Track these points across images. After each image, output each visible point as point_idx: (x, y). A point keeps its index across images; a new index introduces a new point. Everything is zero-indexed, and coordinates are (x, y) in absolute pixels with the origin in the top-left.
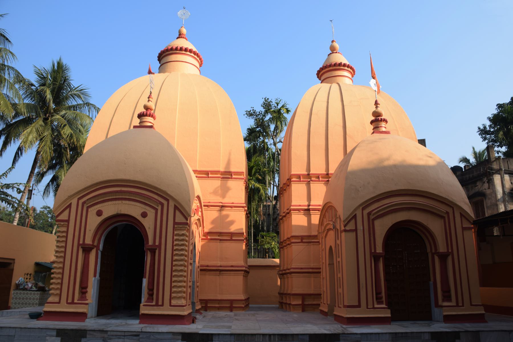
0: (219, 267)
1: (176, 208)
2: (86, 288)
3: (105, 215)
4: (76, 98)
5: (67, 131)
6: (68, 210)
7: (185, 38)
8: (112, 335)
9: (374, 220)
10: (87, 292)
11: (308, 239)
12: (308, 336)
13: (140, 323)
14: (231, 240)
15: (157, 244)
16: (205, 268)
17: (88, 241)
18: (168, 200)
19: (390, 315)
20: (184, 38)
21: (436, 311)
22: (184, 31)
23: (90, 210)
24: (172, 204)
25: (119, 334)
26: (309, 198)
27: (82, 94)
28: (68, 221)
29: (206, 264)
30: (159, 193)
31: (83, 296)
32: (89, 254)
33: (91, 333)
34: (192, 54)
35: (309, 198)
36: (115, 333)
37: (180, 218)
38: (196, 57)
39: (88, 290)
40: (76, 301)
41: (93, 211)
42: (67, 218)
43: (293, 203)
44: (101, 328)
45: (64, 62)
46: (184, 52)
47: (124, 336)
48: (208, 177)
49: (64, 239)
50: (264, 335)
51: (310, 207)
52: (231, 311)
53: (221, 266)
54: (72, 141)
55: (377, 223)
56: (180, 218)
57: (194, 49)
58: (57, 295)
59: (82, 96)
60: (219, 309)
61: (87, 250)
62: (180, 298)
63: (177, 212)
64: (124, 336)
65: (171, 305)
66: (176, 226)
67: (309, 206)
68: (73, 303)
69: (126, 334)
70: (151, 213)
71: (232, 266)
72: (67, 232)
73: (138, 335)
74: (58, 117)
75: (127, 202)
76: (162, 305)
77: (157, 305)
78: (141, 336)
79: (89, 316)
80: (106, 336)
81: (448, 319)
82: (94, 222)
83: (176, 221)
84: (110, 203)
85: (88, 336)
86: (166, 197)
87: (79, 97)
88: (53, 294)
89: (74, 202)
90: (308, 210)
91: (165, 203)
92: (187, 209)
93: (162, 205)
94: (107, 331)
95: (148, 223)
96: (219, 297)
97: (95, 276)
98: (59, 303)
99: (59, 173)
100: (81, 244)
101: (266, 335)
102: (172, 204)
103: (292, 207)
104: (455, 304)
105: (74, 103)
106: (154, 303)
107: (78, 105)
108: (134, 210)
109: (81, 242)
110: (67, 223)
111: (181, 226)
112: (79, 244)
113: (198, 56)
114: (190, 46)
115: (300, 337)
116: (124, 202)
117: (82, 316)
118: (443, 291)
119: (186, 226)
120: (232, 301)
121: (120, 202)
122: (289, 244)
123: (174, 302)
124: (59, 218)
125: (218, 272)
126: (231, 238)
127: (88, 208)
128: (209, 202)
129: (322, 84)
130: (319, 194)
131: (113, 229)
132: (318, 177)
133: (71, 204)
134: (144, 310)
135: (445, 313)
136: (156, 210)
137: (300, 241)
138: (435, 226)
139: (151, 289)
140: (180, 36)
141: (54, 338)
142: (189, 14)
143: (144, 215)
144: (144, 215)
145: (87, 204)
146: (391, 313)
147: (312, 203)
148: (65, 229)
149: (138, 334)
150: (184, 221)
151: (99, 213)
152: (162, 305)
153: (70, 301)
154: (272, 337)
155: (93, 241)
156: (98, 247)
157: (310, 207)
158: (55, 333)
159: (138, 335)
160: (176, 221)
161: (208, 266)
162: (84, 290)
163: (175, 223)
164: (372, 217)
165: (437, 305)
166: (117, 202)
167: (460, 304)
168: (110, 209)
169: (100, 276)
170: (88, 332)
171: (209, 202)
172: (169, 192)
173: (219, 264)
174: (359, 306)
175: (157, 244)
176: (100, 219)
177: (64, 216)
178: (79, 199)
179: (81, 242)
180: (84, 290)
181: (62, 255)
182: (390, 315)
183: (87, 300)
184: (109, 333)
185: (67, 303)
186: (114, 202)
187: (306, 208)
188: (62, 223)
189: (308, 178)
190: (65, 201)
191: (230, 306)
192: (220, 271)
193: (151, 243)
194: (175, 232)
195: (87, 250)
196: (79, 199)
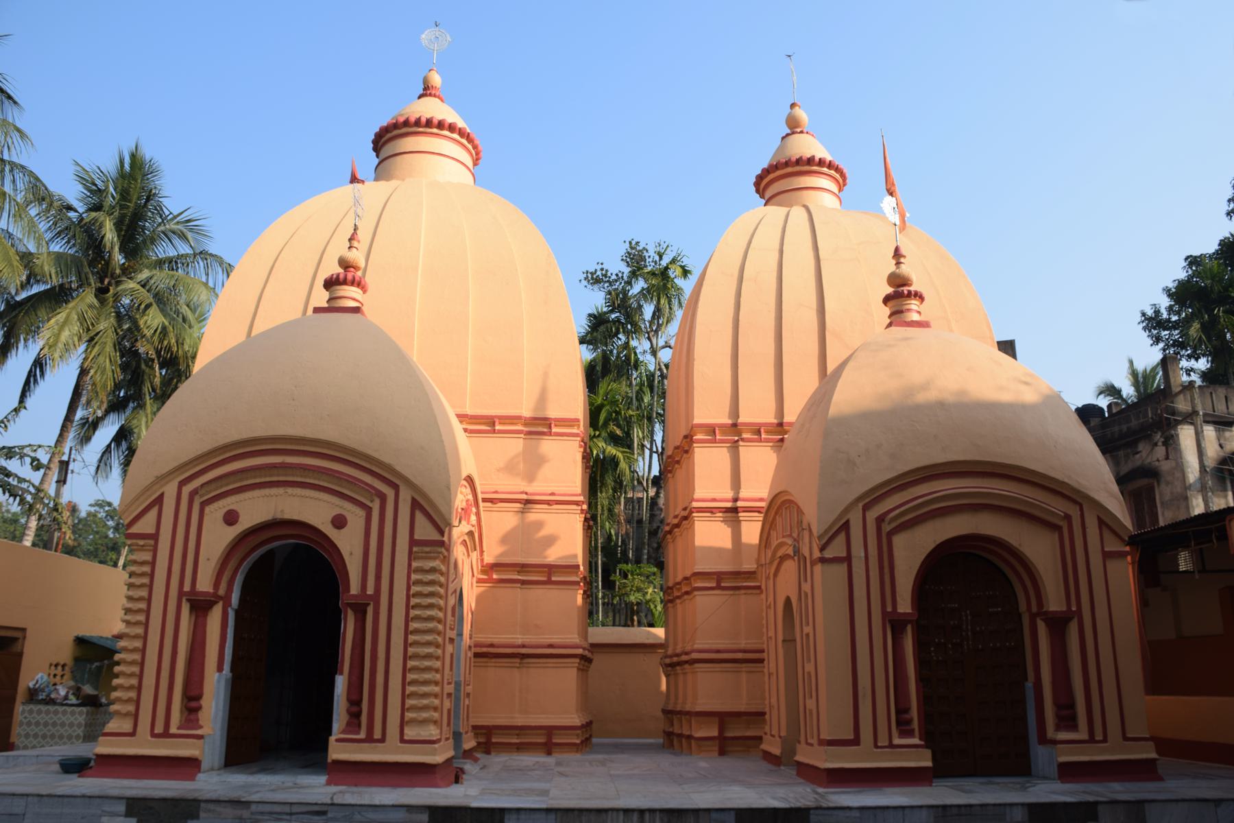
0: (519, 647)
1: (415, 505)
2: (199, 697)
3: (245, 523)
4: (176, 241)
5: (153, 318)
6: (153, 513)
7: (439, 97)
8: (262, 813)
9: (891, 534)
10: (199, 708)
11: (733, 580)
12: (733, 813)
13: (329, 783)
14: (549, 582)
15: (370, 591)
16: (485, 650)
17: (205, 584)
18: (396, 487)
19: (929, 764)
20: (435, 96)
21: (1041, 755)
22: (436, 79)
23: (207, 509)
24: (405, 496)
25: (278, 809)
26: (736, 483)
27: (191, 230)
28: (155, 537)
29: (489, 641)
30: (374, 469)
31: (192, 717)
32: (205, 616)
33: (211, 806)
34: (455, 136)
35: (736, 483)
36: (267, 808)
37: (424, 530)
38: (464, 141)
39: (204, 702)
40: (173, 730)
41: (215, 513)
42: (152, 530)
43: (698, 494)
44: (234, 795)
45: (147, 153)
46: (435, 130)
47: (291, 814)
48: (494, 431)
49: (146, 580)
50: (627, 811)
51: (739, 504)
52: (549, 753)
53: (524, 646)
54: (165, 343)
55: (899, 541)
56: (424, 530)
57: (461, 124)
58: (127, 714)
59: (189, 235)
60: (520, 748)
61: (200, 606)
62: (424, 722)
63: (419, 515)
64: (291, 814)
65: (402, 741)
66: (415, 549)
67: (736, 500)
68: (166, 734)
69: (295, 809)
70: (356, 518)
71: (551, 646)
72: (153, 564)
73: (324, 813)
74: (131, 285)
75: (298, 491)
76: (383, 740)
77: (369, 739)
78: (330, 815)
79: (204, 766)
80: (245, 814)
81: (1068, 772)
82: (217, 539)
83: (416, 537)
84: (256, 493)
85: (202, 815)
86: (392, 479)
87: (183, 237)
88: (117, 713)
89: (170, 490)
90: (735, 510)
91: (390, 493)
92: (443, 509)
93: (383, 498)
94: (247, 804)
95: (348, 543)
96: (520, 721)
97: (220, 669)
98: (133, 734)
99: (135, 422)
100: (187, 594)
101: (633, 810)
102: (405, 496)
103: (695, 504)
104: (1085, 736)
105: (172, 253)
106: (362, 735)
107: (180, 256)
108: (313, 509)
109: (187, 588)
110: (152, 542)
111: (427, 549)
112: (181, 593)
113: (470, 140)
114: (451, 116)
115: (714, 815)
116: (290, 490)
117: (188, 766)
118: (1058, 705)
119: (440, 549)
120: (550, 730)
121: (281, 490)
122: (687, 593)
123: (410, 733)
124: (134, 530)
125: (518, 660)
126: (549, 578)
127: (204, 505)
128: (496, 492)
129: (768, 207)
130: (760, 472)
131: (262, 557)
132: (759, 432)
133: (162, 495)
134: (338, 752)
135: (1063, 759)
136: (369, 510)
137: (714, 585)
138: (1038, 549)
139: (354, 702)
140: (427, 91)
141: (122, 819)
142: (449, 39)
143: (339, 522)
144: (339, 522)
145: (201, 496)
146: (934, 759)
147: (742, 494)
148: (147, 556)
149: (324, 808)
150: (435, 536)
151: (231, 518)
152: (383, 740)
153: (159, 729)
154: (647, 815)
155: (217, 585)
156: (227, 600)
157: (739, 504)
158: (122, 808)
159: (324, 813)
160: (416, 537)
161: (492, 645)
162: (193, 704)
163: (413, 542)
164: (887, 528)
165: (1043, 740)
166: (274, 491)
167: (1099, 737)
168: (256, 508)
169: (232, 670)
170: (203, 805)
171: (496, 492)
172: (398, 468)
173: (520, 642)
174: (856, 741)
175: (370, 591)
176: (232, 532)
177: (146, 525)
178: (182, 483)
179: (187, 588)
180: (193, 704)
181: (141, 618)
182: (929, 764)
183: (201, 727)
184: (253, 807)
185: (153, 735)
186: (267, 491)
187: (729, 505)
188: (141, 542)
189: (734, 433)
190: (147, 489)
191: (547, 741)
192: (521, 657)
193: (354, 589)
194: (415, 564)
195: (200, 606)
196: (182, 483)
